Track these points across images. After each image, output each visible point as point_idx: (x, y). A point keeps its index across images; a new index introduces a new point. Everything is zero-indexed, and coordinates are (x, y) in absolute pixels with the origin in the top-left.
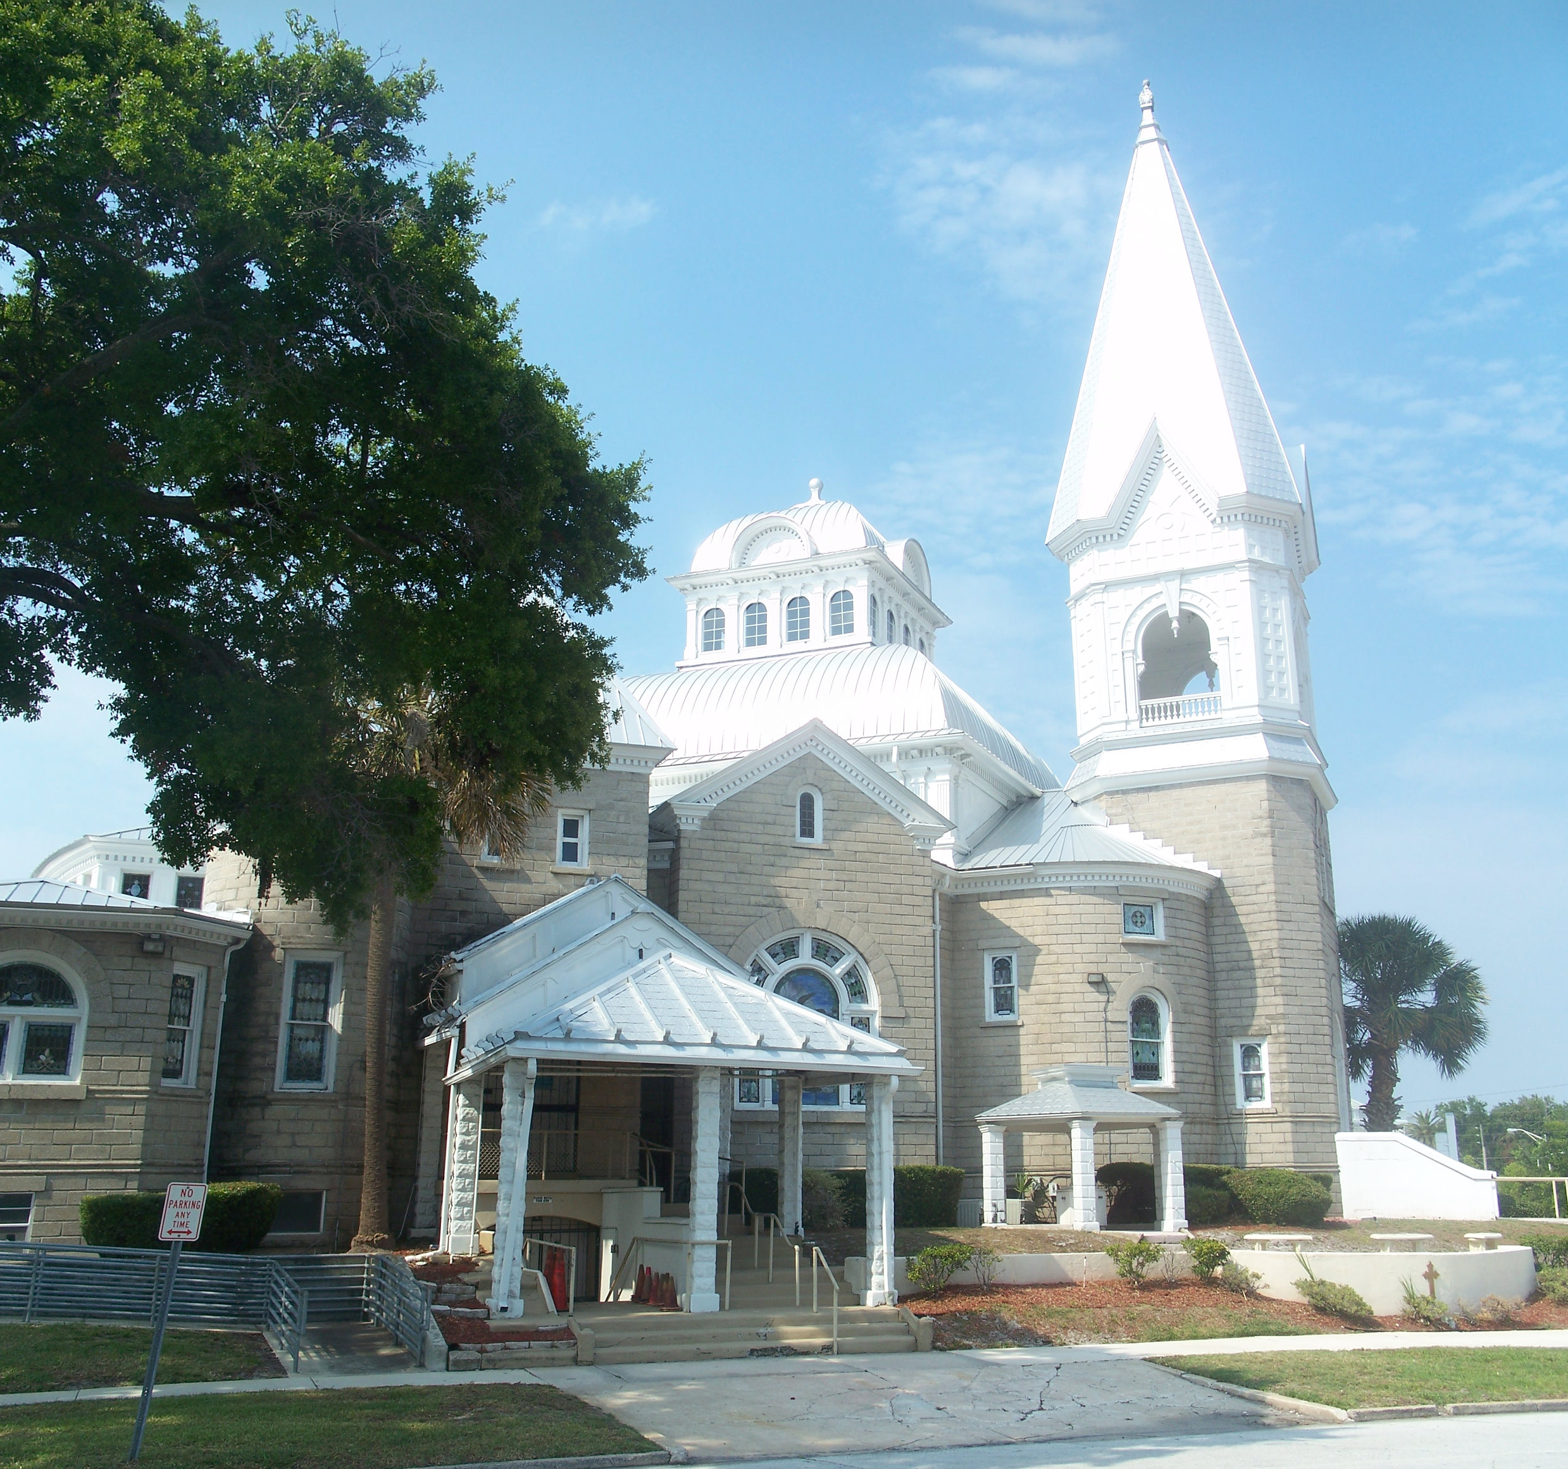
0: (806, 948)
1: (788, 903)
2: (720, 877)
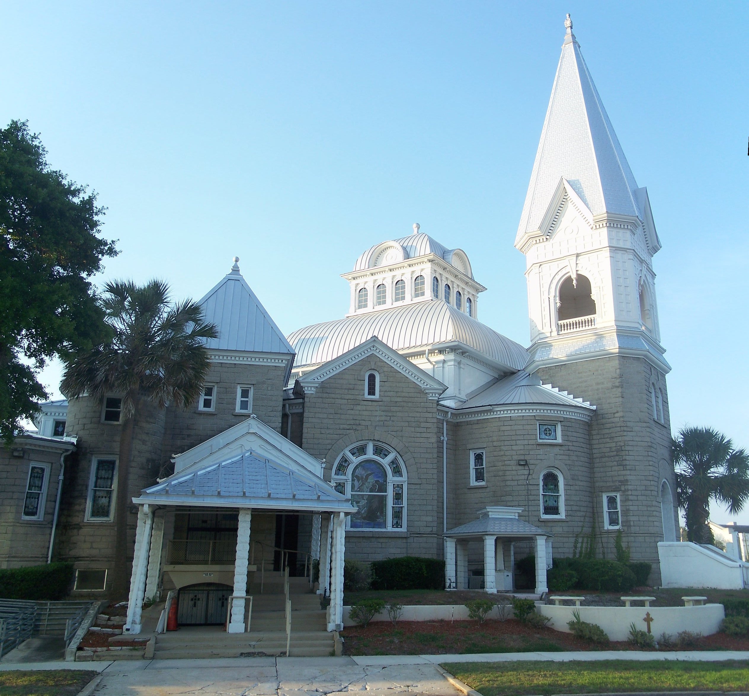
0: (370, 448)
2: (325, 416)
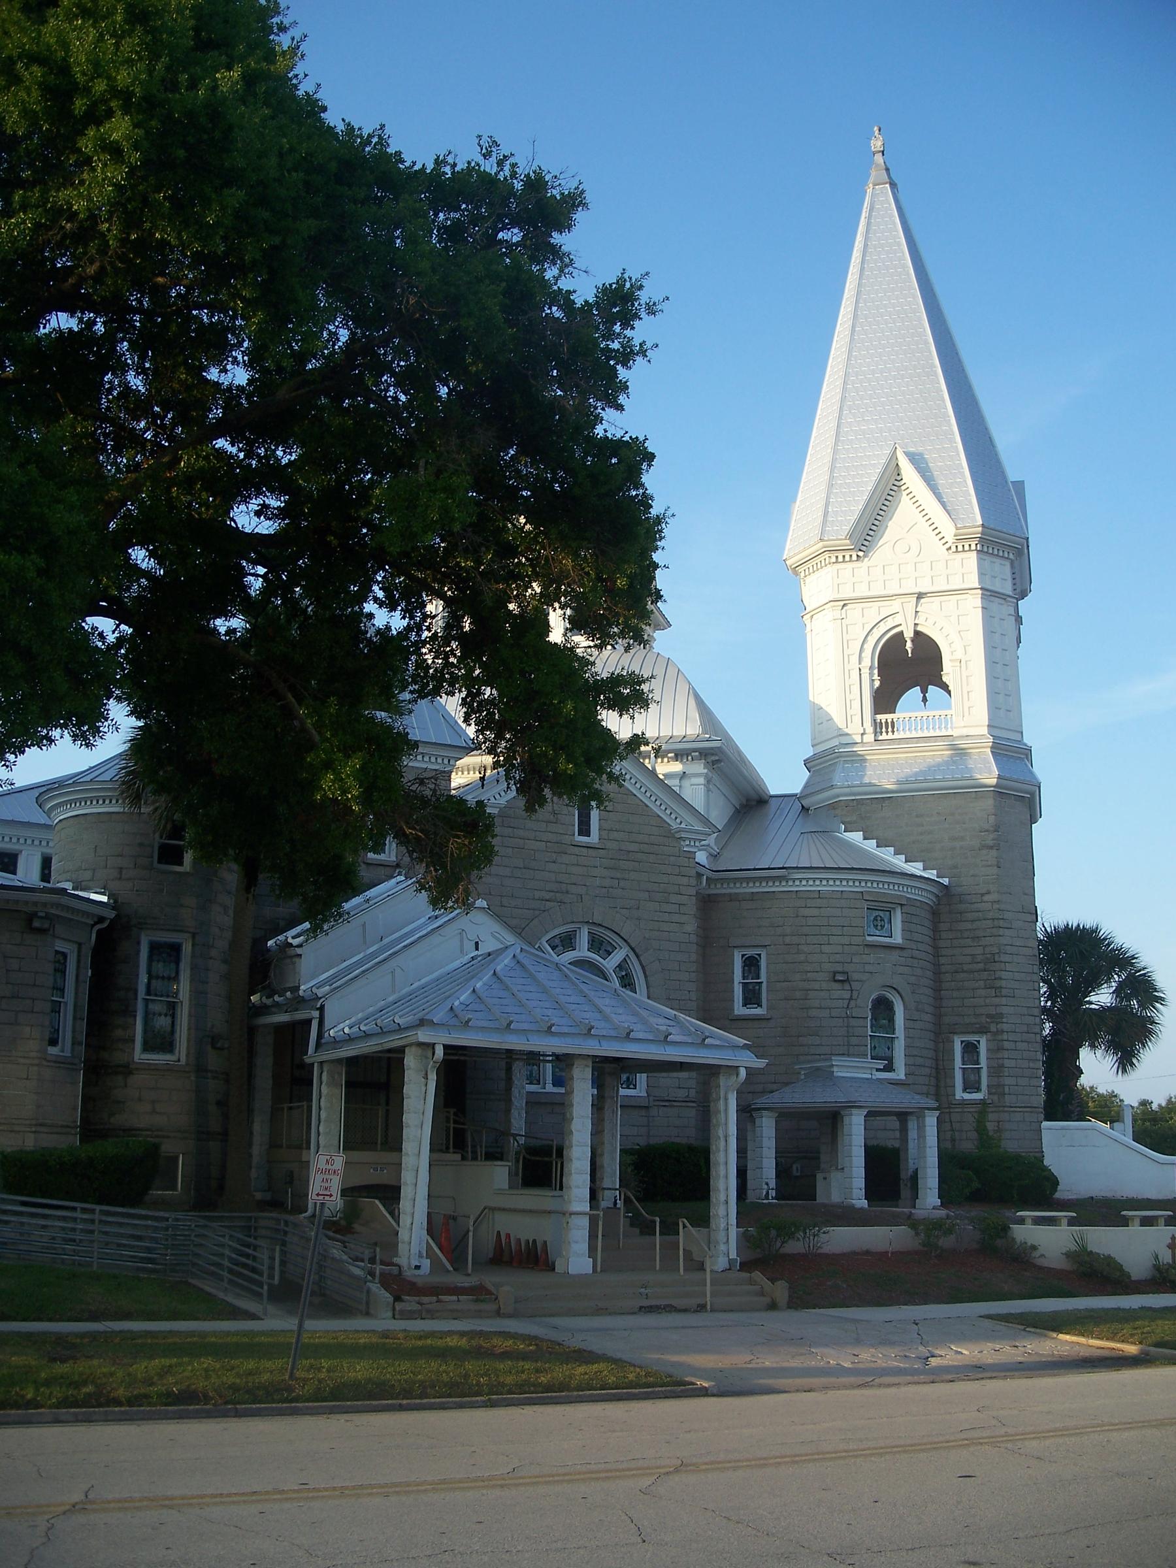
0: (583, 939)
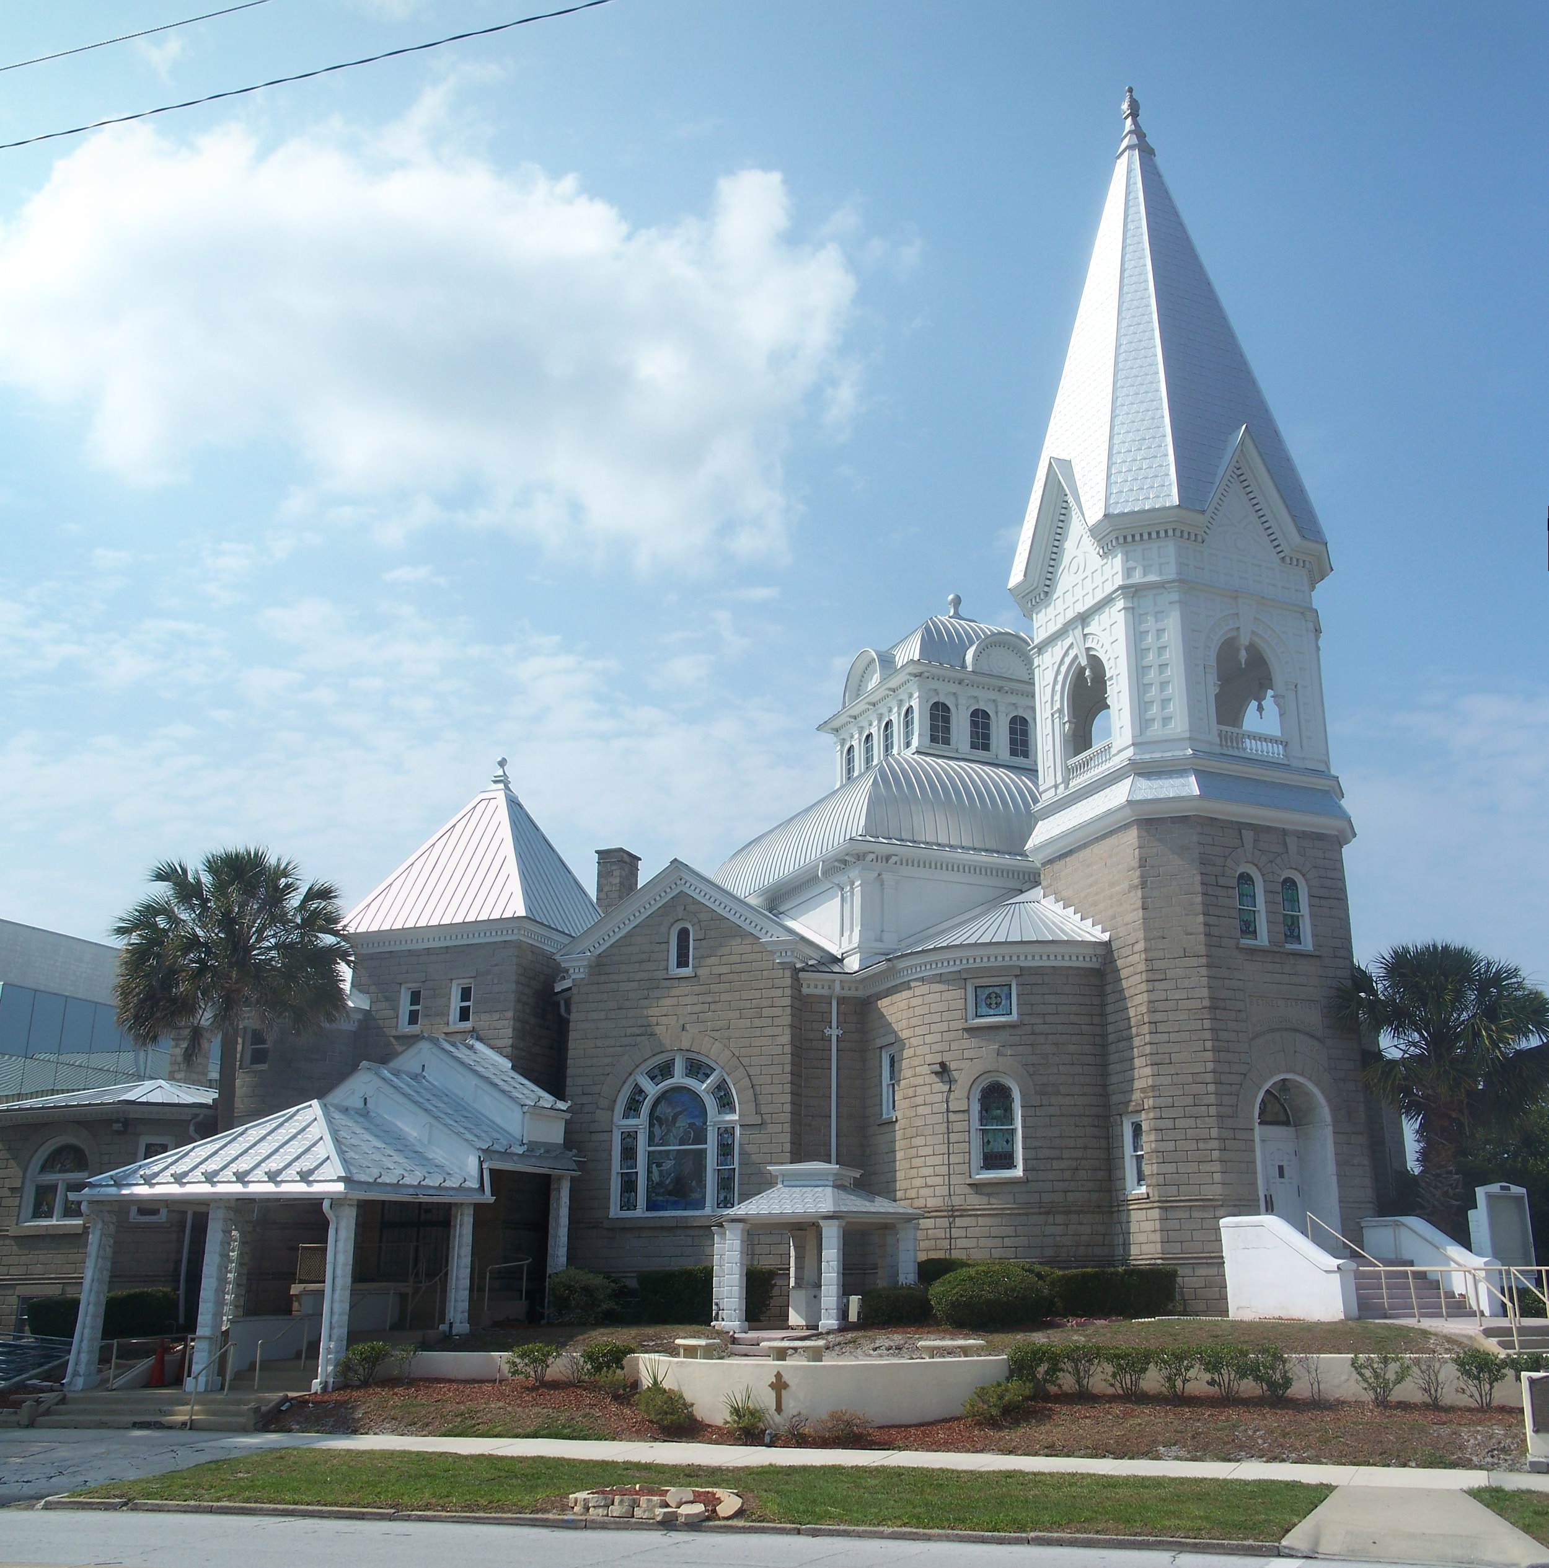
0: (679, 1067)
1: (658, 1030)
2: (602, 1015)
